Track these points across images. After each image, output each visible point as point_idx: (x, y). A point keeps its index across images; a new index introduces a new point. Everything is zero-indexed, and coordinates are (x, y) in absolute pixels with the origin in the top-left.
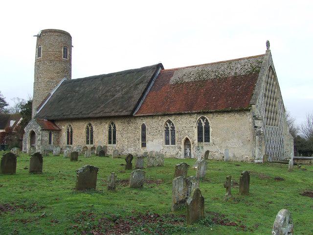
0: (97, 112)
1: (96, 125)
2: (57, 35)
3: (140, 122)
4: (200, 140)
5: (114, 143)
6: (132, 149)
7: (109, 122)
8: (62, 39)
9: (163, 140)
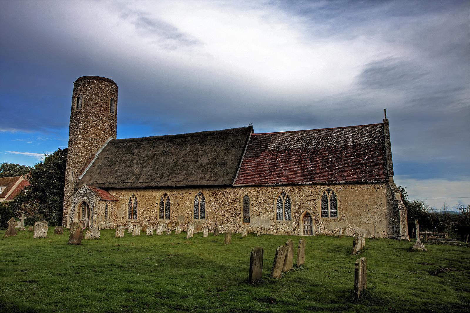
0: (179, 179)
3: (241, 193)
4: (325, 215)
5: (203, 217)
6: (229, 225)
7: (195, 193)
8: (110, 88)
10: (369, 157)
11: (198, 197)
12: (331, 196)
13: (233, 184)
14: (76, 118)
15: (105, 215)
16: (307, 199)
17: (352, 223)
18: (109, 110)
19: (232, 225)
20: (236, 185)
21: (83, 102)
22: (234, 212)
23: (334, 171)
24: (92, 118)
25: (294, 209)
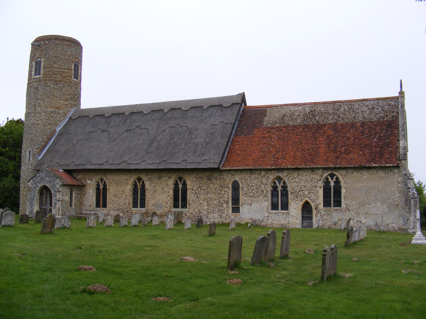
1: (151, 180)
2: (67, 45)
3: (229, 180)
4: (327, 203)
6: (216, 215)
9: (267, 204)
10: (380, 137)
11: (179, 183)
12: (335, 182)
13: (221, 166)
14: (34, 85)
15: (69, 202)
16: (307, 186)
17: (358, 214)
18: (73, 76)
19: (219, 215)
20: (224, 168)
21: (42, 66)
22: (222, 201)
23: (339, 153)
24: (52, 86)
25: (292, 197)
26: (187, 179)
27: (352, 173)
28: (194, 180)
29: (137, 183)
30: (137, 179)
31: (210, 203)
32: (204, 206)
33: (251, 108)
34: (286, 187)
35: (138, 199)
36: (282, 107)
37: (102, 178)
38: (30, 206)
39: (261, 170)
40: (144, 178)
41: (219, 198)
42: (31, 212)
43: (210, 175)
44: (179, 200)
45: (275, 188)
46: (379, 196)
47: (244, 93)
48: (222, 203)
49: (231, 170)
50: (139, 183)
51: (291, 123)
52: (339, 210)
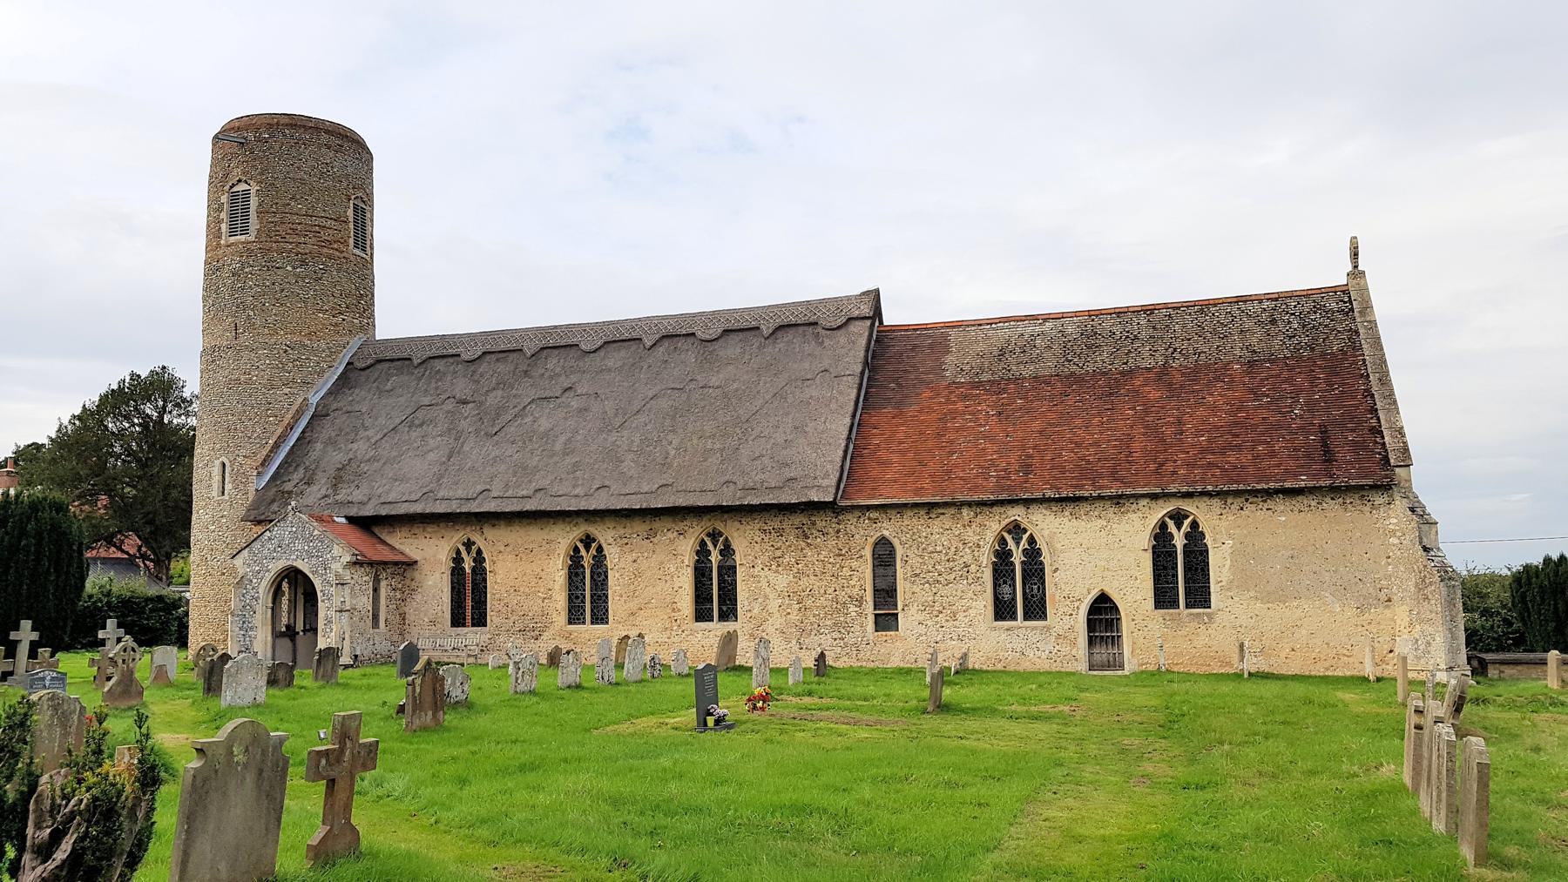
3: (863, 534)
4: (1164, 598)
11: (710, 546)
12: (1187, 535)
18: (351, 241)
19: (835, 639)
20: (848, 503)
24: (289, 268)
26: (736, 534)
27: (1242, 509)
28: (756, 538)
29: (579, 551)
30: (581, 541)
31: (809, 603)
32: (789, 613)
33: (901, 330)
34: (1038, 552)
35: (584, 597)
36: (994, 326)
37: (469, 539)
38: (242, 633)
39: (963, 504)
40: (605, 535)
41: (835, 591)
42: (243, 649)
43: (803, 524)
44: (712, 597)
45: (1003, 556)
46: (1327, 574)
47: (877, 291)
48: (844, 603)
49: (869, 508)
50: (588, 552)
51: (1028, 371)
52: (1205, 618)
